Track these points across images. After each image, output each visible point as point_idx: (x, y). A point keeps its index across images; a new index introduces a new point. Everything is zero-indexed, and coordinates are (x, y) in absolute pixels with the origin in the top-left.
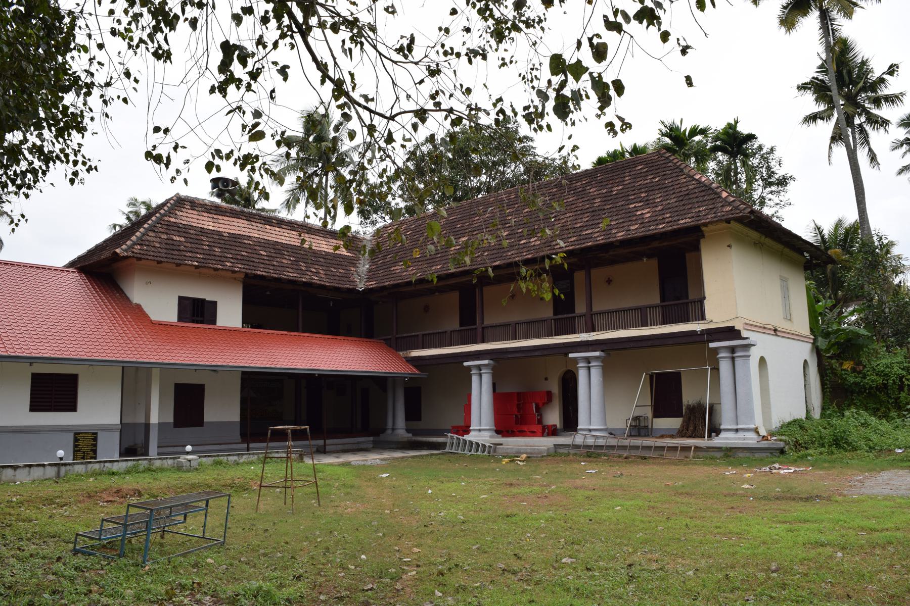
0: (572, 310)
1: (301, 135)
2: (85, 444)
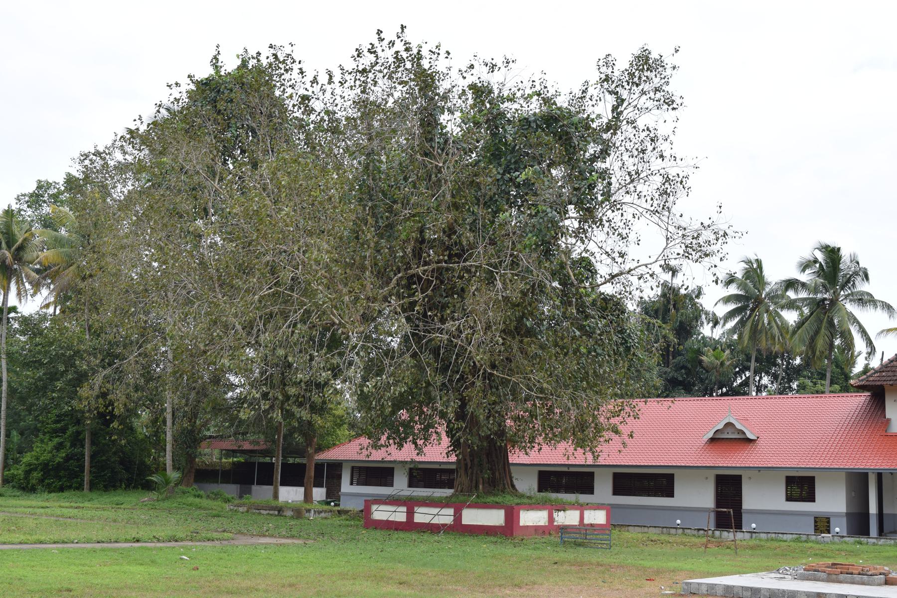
0: (284, 483)
1: (416, 509)
2: (822, 524)
